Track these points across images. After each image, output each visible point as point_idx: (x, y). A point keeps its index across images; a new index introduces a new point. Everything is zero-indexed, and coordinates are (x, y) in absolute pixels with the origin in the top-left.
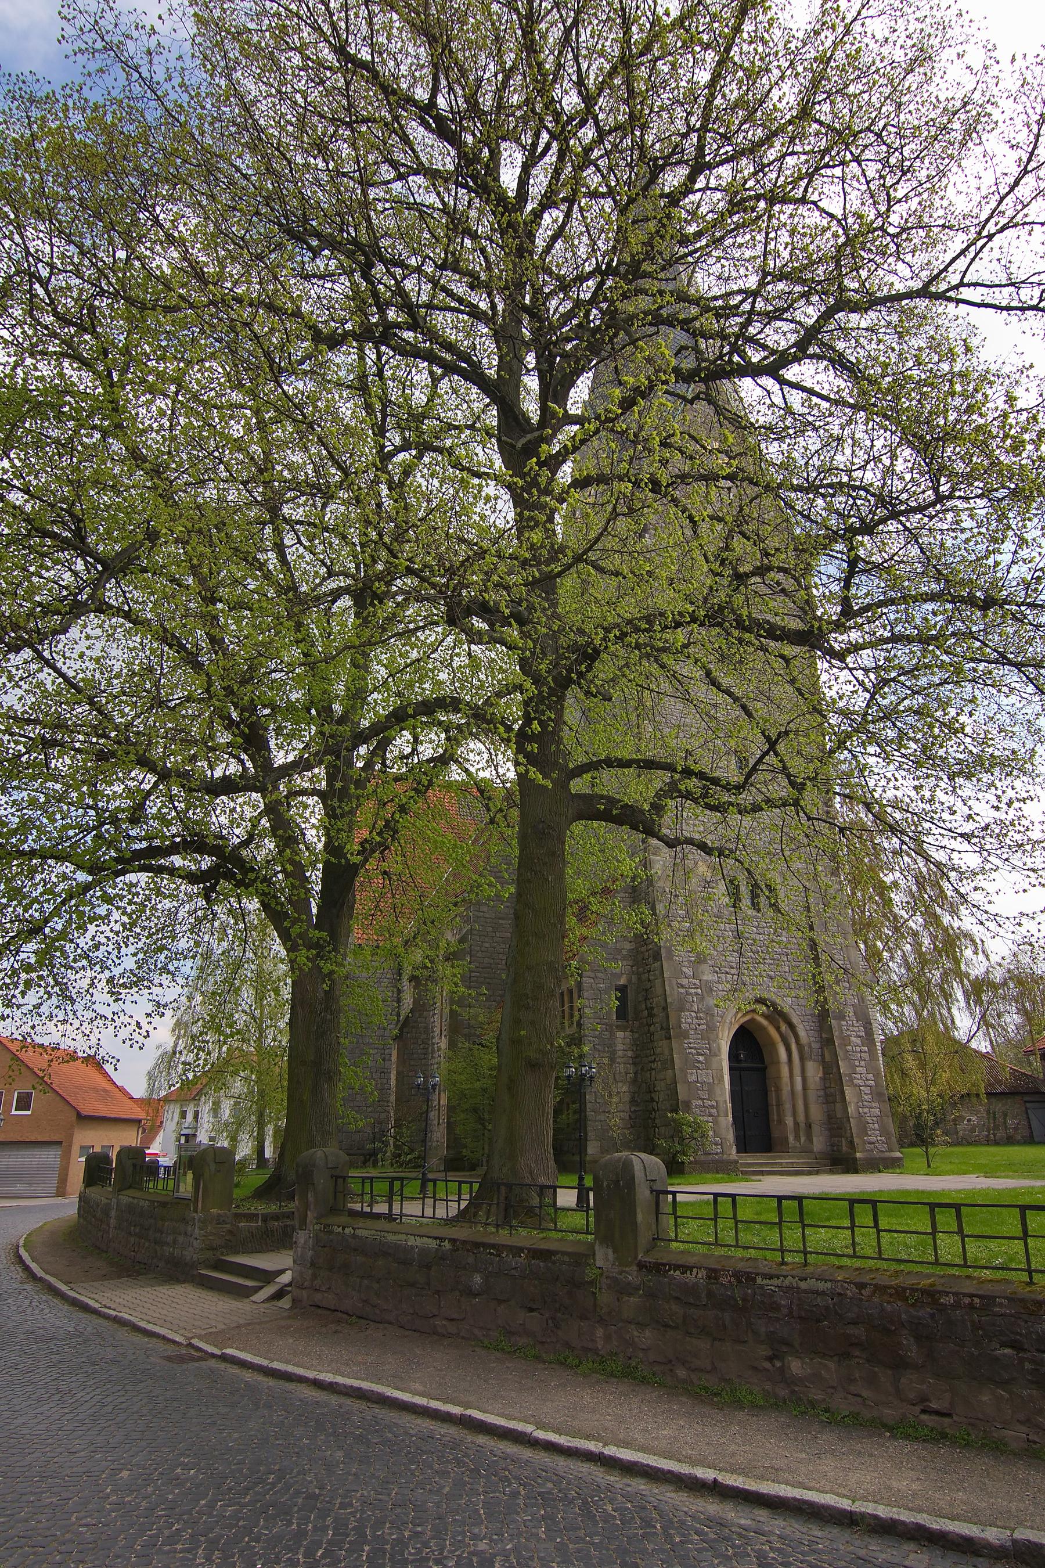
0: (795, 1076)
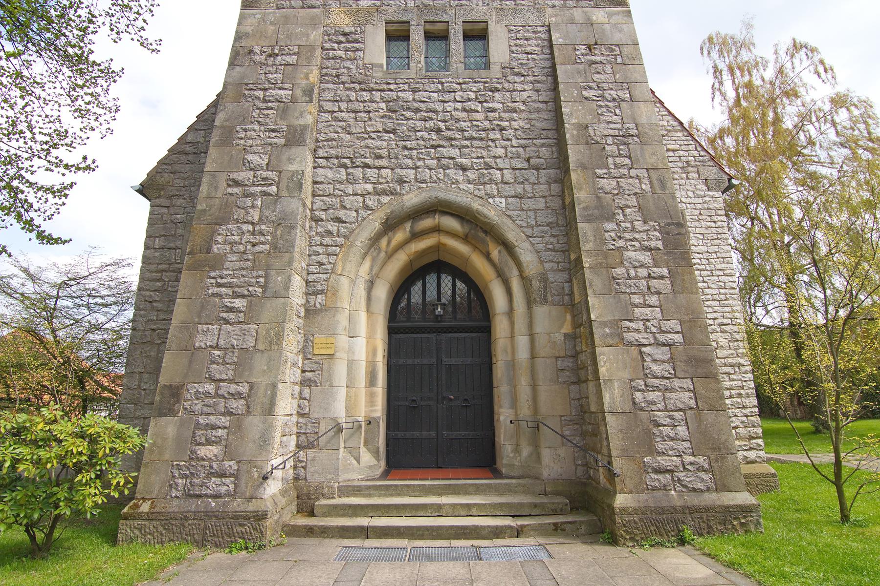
0: (521, 335)
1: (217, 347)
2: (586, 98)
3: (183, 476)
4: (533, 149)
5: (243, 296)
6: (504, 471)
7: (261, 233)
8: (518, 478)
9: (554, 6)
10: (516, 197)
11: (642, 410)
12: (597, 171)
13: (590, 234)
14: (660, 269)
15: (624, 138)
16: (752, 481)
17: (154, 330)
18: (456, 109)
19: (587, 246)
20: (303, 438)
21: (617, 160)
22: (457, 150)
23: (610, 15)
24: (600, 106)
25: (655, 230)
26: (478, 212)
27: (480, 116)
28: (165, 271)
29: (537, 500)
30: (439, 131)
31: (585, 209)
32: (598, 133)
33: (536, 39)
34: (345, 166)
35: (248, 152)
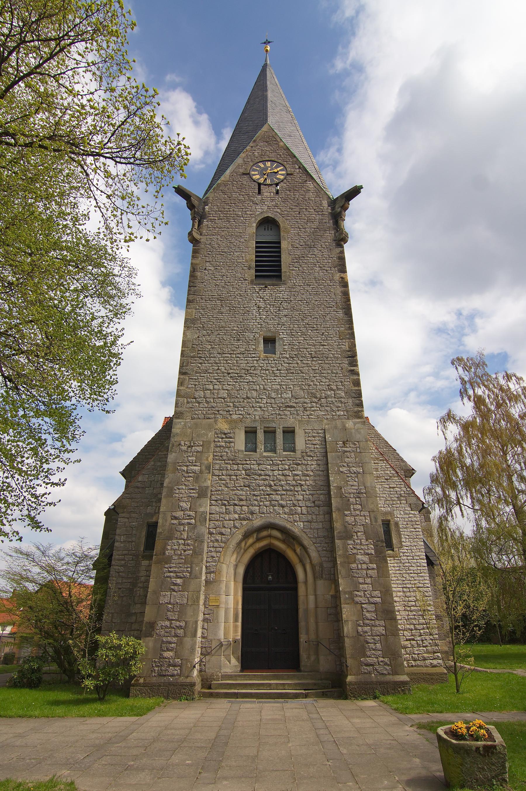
0: (310, 595)
1: (170, 603)
2: (342, 472)
3: (157, 666)
4: (316, 496)
5: (181, 578)
6: (302, 669)
7: (188, 545)
8: (309, 672)
9: (327, 419)
10: (308, 522)
11: (361, 635)
12: (345, 512)
13: (341, 546)
16: (434, 677)
17: (120, 588)
18: (279, 475)
19: (339, 552)
20: (204, 650)
22: (280, 496)
23: (355, 424)
24: (348, 476)
26: (289, 529)
27: (290, 478)
28: (126, 555)
29: (317, 682)
30: (270, 486)
31: (339, 532)
32: (346, 491)
33: (318, 436)
34: (225, 505)
35: (180, 501)
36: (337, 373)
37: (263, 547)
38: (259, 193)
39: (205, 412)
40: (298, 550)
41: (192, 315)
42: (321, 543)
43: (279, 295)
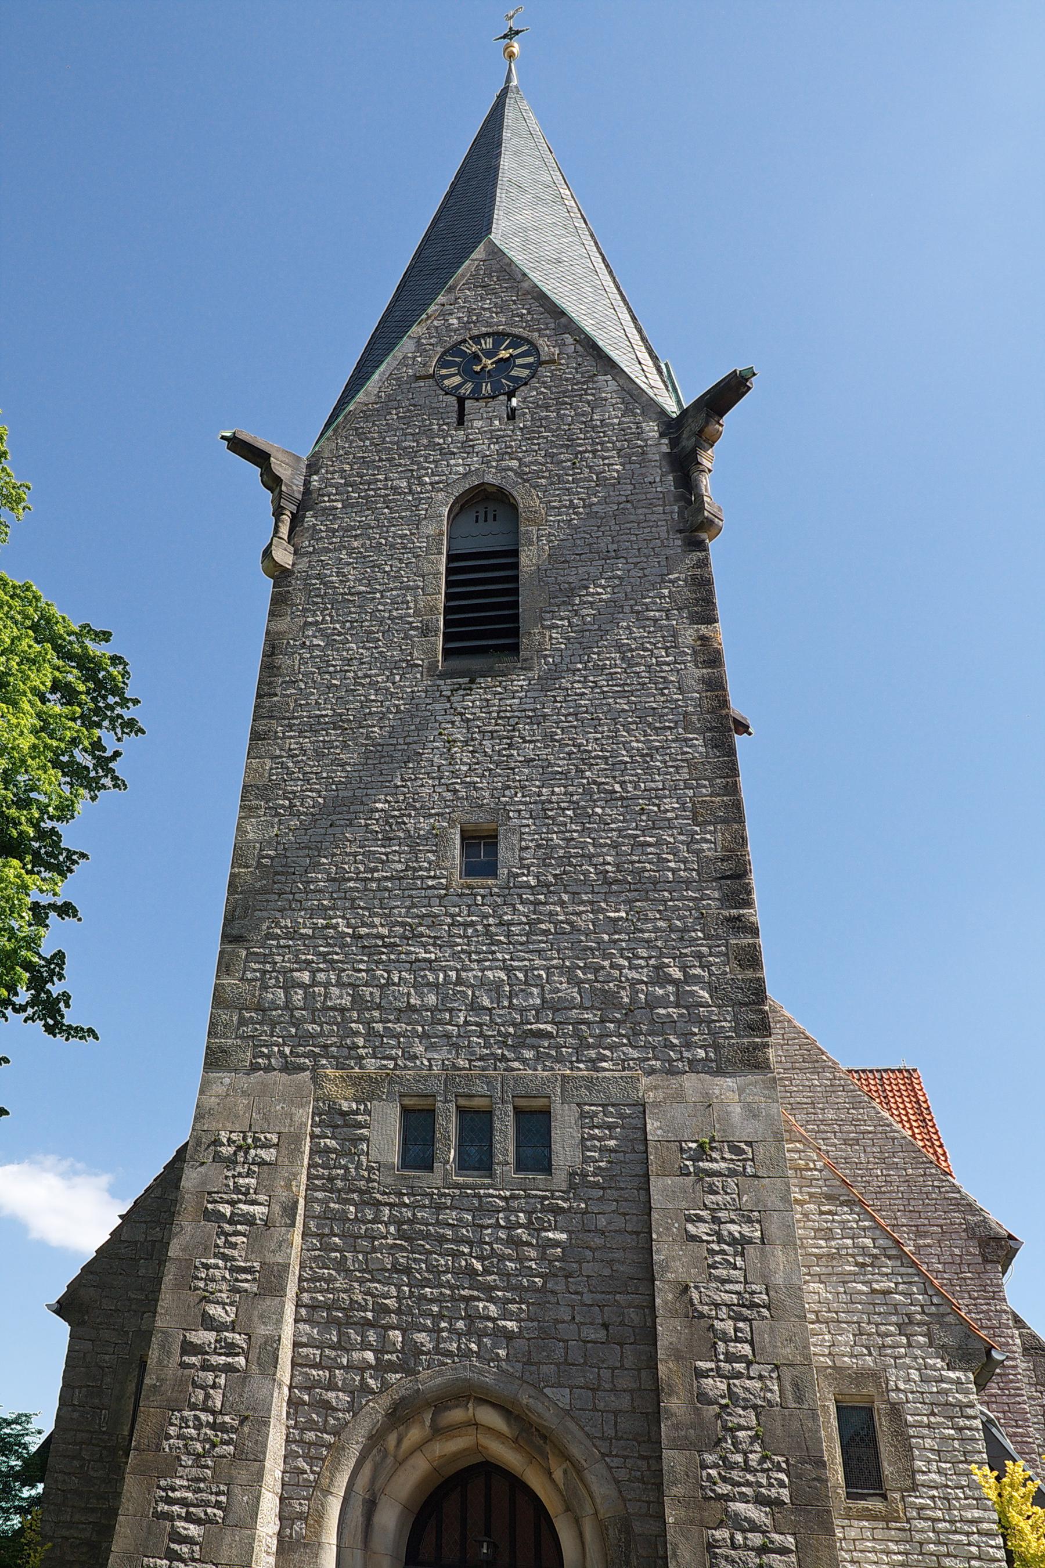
12: (699, 1364)
14: (782, 1537)
15: (744, 1309)
21: (732, 1347)
25: (780, 1470)
36: (685, 930)
37: (455, 1456)
38: (461, 421)
39: (287, 1050)
40: (558, 1475)
41: (261, 776)
42: (625, 1457)
43: (508, 702)
